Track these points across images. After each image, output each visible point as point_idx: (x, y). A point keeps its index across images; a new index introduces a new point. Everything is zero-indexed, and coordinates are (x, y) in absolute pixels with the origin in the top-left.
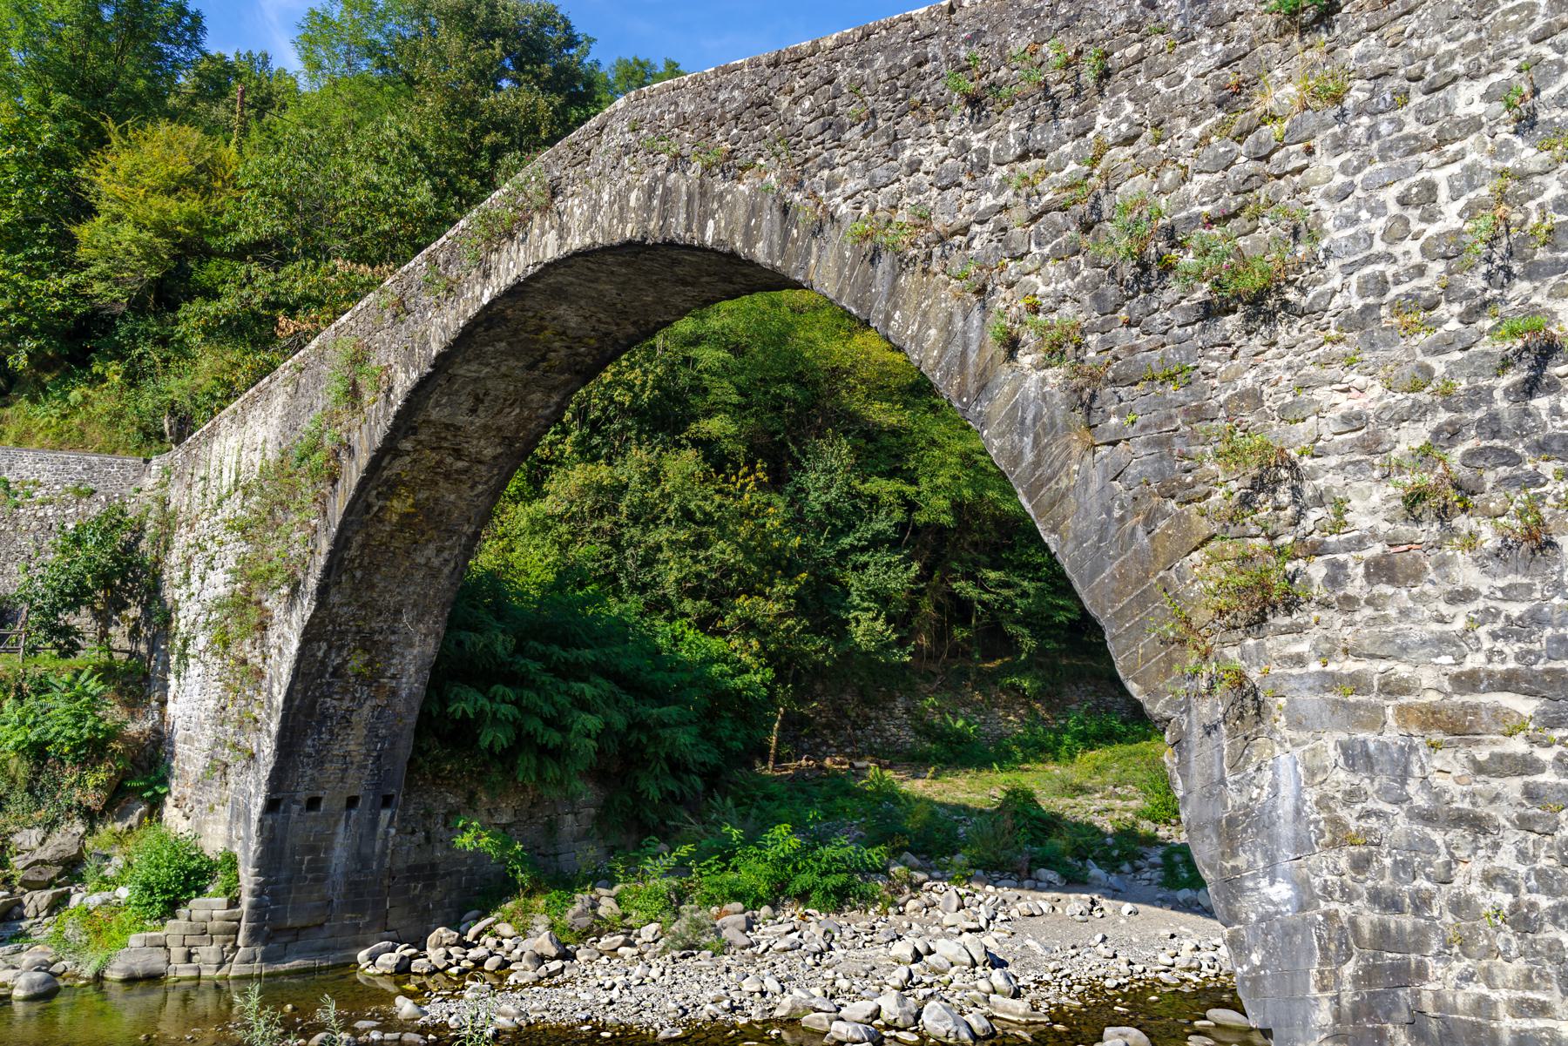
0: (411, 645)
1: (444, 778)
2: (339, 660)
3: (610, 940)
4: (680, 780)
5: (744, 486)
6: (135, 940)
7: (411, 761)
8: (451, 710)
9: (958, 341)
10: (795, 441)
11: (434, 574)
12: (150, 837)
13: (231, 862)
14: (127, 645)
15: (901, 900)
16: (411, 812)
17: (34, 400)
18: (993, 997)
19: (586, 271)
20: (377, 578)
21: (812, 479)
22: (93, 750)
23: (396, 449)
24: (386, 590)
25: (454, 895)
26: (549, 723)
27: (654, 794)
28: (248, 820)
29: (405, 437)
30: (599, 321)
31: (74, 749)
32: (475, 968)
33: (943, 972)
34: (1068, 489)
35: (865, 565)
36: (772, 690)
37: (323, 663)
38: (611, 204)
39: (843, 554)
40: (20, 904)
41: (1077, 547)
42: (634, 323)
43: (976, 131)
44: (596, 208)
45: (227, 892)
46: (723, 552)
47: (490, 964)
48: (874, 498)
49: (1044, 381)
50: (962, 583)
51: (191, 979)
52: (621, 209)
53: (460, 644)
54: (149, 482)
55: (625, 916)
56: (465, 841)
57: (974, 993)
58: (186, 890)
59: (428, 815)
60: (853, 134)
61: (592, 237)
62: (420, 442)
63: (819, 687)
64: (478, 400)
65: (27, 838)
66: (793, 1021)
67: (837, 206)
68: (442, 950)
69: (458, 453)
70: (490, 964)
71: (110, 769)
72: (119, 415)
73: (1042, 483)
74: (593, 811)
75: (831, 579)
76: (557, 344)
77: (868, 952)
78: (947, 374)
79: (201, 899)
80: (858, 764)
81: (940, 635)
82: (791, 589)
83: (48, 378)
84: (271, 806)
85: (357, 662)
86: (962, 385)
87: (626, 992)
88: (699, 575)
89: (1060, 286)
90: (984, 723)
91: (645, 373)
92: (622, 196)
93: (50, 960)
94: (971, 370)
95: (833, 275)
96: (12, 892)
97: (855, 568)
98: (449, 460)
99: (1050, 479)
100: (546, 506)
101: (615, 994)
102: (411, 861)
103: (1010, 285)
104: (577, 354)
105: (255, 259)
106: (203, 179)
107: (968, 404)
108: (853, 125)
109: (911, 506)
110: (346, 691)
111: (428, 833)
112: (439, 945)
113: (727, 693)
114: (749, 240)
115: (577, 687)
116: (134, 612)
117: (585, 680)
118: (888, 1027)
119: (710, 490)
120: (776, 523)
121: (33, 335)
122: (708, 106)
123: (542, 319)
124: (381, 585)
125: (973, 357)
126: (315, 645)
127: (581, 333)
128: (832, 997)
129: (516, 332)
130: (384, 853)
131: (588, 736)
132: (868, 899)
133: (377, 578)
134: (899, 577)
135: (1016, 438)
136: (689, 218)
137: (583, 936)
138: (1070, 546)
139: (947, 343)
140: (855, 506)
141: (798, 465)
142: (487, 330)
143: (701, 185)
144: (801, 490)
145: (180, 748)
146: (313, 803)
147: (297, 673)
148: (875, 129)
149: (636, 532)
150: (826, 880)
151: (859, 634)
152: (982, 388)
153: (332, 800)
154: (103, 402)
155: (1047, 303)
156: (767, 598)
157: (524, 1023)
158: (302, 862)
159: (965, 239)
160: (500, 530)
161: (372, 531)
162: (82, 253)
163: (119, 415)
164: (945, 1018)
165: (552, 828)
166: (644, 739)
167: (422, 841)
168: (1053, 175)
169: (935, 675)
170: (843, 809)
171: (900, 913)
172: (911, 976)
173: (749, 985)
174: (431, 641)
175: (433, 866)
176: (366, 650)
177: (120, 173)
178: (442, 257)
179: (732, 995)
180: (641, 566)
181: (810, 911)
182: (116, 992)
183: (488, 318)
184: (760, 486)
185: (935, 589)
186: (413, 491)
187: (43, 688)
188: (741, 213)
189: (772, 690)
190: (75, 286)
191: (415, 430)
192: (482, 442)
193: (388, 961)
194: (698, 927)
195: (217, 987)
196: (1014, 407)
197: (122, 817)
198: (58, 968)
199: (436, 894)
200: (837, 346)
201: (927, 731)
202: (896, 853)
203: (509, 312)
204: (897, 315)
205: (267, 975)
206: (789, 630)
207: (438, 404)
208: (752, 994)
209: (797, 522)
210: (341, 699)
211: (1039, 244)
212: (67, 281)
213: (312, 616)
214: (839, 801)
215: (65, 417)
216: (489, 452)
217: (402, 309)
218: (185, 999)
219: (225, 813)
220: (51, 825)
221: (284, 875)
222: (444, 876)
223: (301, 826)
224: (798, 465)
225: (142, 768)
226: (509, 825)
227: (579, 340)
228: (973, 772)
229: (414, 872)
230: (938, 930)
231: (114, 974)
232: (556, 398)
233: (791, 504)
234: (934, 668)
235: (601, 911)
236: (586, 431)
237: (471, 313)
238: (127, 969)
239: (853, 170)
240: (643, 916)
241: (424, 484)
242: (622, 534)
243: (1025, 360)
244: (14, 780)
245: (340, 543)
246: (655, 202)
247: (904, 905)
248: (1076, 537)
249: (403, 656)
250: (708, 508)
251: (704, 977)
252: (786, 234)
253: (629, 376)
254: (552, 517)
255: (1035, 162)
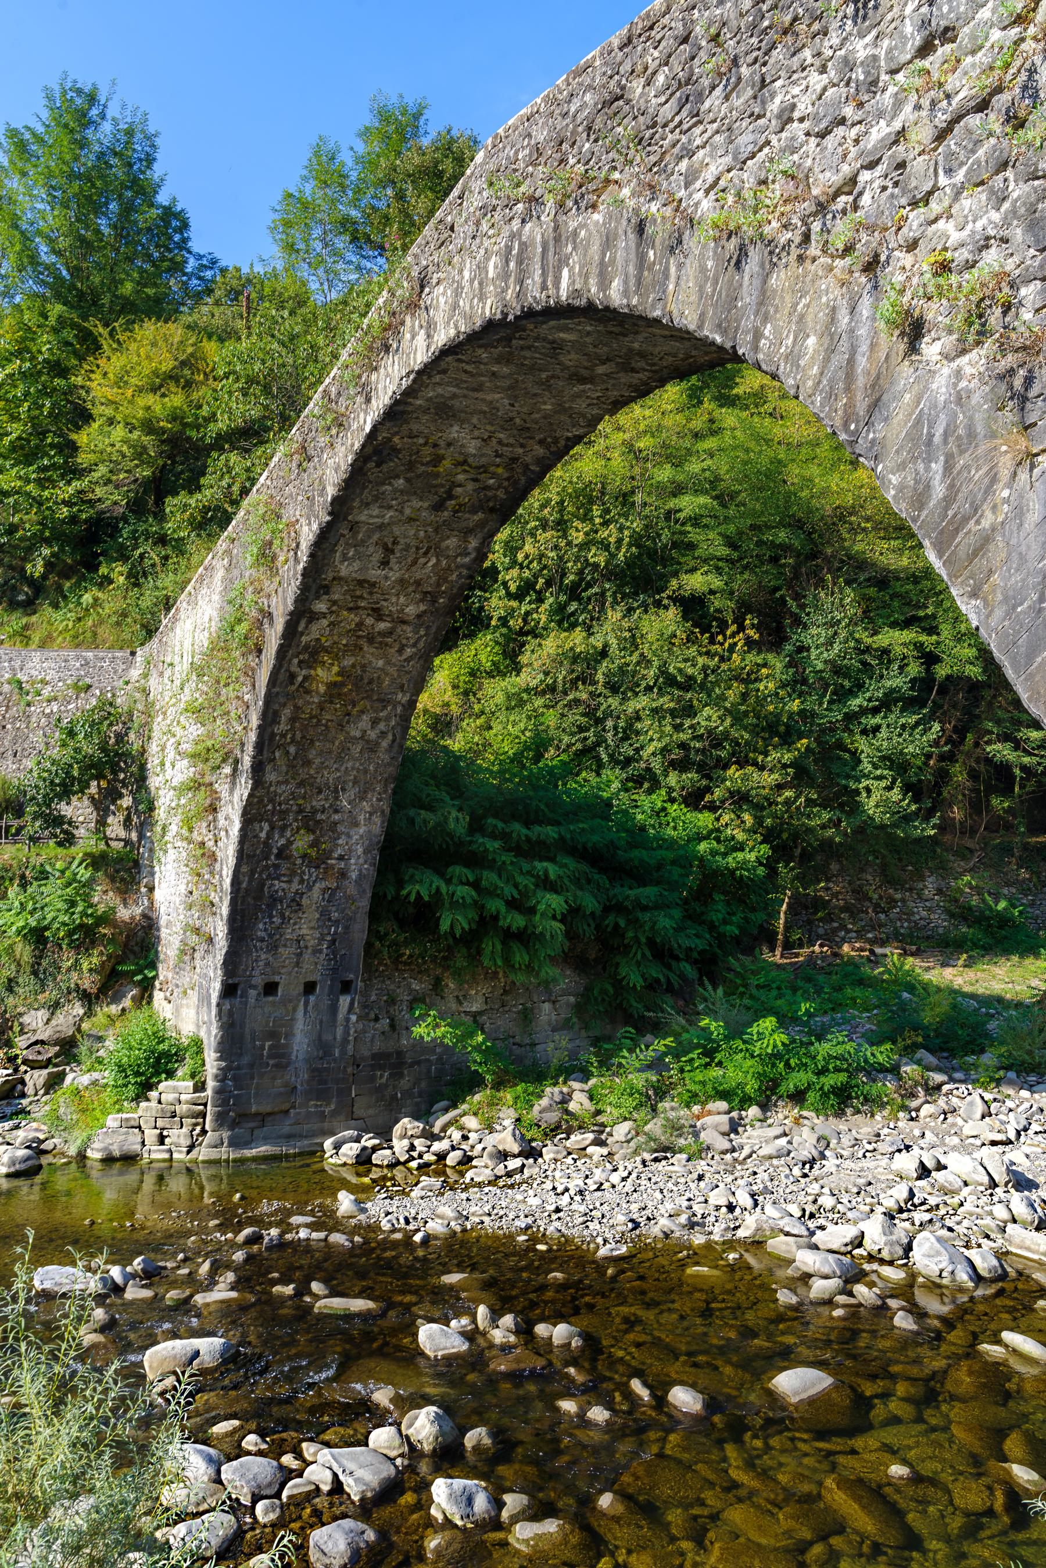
0: (356, 824)
1: (405, 963)
2: (282, 841)
3: (580, 1137)
4: (669, 967)
5: (732, 648)
6: (112, 1121)
7: (369, 946)
8: (404, 892)
9: (844, 346)
10: (797, 597)
11: (372, 747)
12: (137, 1024)
13: (198, 1045)
14: (122, 834)
15: (914, 1104)
16: (373, 998)
17: (56, 606)
18: (1010, 1228)
19: (464, 377)
20: (312, 754)
21: (815, 634)
22: (85, 936)
23: (311, 612)
24: (322, 766)
25: (423, 1085)
26: (513, 904)
27: (635, 979)
28: (209, 1004)
29: (318, 598)
30: (500, 442)
31: (70, 933)
32: (437, 1162)
33: (953, 1192)
34: (993, 529)
35: (877, 729)
36: (772, 872)
37: (266, 843)
38: (472, 281)
39: (851, 717)
40: (23, 1083)
41: (1008, 615)
42: (541, 442)
43: (862, 35)
44: (457, 293)
45: (193, 1076)
46: (709, 719)
47: (452, 1159)
48: (886, 651)
49: (958, 374)
50: (998, 746)
51: (164, 1160)
52: (481, 284)
53: (412, 821)
54: (135, 673)
55: (598, 1112)
56: (420, 1030)
57: (988, 1221)
58: (157, 1073)
59: (392, 1001)
60: (713, 101)
61: (456, 327)
62: (334, 603)
63: (834, 867)
64: (388, 551)
65: (36, 1020)
66: (759, 1243)
67: (697, 204)
68: (406, 1142)
69: (378, 614)
70: (452, 1159)
71: (101, 954)
72: (124, 615)
73: (958, 525)
74: (572, 999)
75: (840, 746)
76: (461, 477)
77: (864, 1163)
78: (831, 396)
79: (170, 1083)
80: (879, 951)
81: (977, 805)
82: (787, 757)
83: (68, 584)
84: (229, 991)
85: (301, 843)
86: (850, 406)
87: (578, 1198)
88: (683, 746)
89: (979, 225)
90: (1032, 904)
91: (621, 529)
92: (482, 268)
93: (42, 1137)
94: (861, 381)
95: (694, 298)
96: (16, 1070)
97: (864, 732)
98: (370, 621)
99: (966, 519)
100: (527, 678)
101: (566, 1198)
102: (376, 1049)
103: (912, 246)
104: (487, 488)
105: (233, 448)
106: (184, 374)
107: (857, 433)
108: (713, 88)
109: (930, 659)
110: (293, 873)
111: (392, 1020)
112: (403, 1136)
113: (717, 873)
114: (604, 284)
115: (540, 866)
116: (127, 801)
117: (552, 860)
118: (871, 1258)
119: (692, 651)
120: (771, 685)
121: (48, 542)
122: (560, 123)
123: (435, 445)
124: (318, 761)
125: (862, 362)
126: (257, 826)
127: (484, 461)
128: (812, 1216)
129: (411, 466)
130: (345, 1041)
131: (554, 917)
132: (873, 1103)
133: (312, 754)
134: (919, 739)
135: (921, 467)
136: (544, 275)
137: (552, 1132)
138: (999, 613)
139: (831, 351)
140: (864, 663)
141: (797, 621)
142: (378, 465)
143: (556, 228)
144: (801, 649)
145: (164, 933)
146: (271, 988)
147: (242, 855)
148: (739, 79)
149: (614, 702)
150: (823, 1079)
151: (870, 805)
152: (875, 405)
153: (289, 985)
154: (111, 602)
155: (963, 255)
156: (762, 768)
157: (458, 1229)
158: (262, 1048)
159: (851, 198)
160: (477, 707)
161: (300, 703)
162: (83, 459)
163: (124, 615)
164: (938, 1254)
165: (527, 1016)
166: (622, 923)
167: (387, 1028)
168: (969, 59)
169: (971, 851)
170: (854, 999)
171: (912, 1119)
172: (912, 1194)
173: (717, 1198)
174: (377, 819)
175: (400, 1054)
176: (310, 831)
177: (111, 376)
178: (333, 390)
179: (696, 1208)
180: (623, 739)
181: (805, 1113)
182: (95, 1168)
183: (374, 453)
184: (749, 642)
185: (969, 755)
186: (336, 658)
187: (43, 875)
188: (595, 248)
189: (772, 871)
190: (80, 492)
191: (326, 589)
192: (402, 599)
193: (350, 1150)
194: (676, 1128)
195: (188, 1170)
196: (918, 422)
197: (116, 999)
198: (47, 1146)
199: (405, 1083)
200: (834, 482)
201: (963, 914)
202: (909, 1051)
203: (396, 439)
204: (768, 330)
205: (235, 1161)
206: (788, 802)
207: (345, 558)
208: (718, 1208)
209: (798, 684)
210: (289, 882)
211: (949, 172)
212: (76, 484)
213: (250, 795)
214: (849, 991)
215: (79, 619)
216: (411, 610)
217: (305, 455)
218: (161, 1178)
219: (193, 996)
220: (54, 1007)
221: (246, 1060)
222: (412, 1065)
223: (260, 1013)
224: (797, 621)
225: (134, 953)
226: (481, 1013)
227: (483, 469)
228: (1015, 958)
229: (380, 1060)
230: (956, 1140)
231: (94, 1154)
232: (473, 543)
233: (789, 665)
234: (970, 843)
235: (572, 1106)
236: (563, 598)
237: (357, 446)
238: (105, 1149)
239: (714, 148)
240: (616, 1113)
241: (347, 650)
242: (600, 704)
243: (931, 349)
244: (19, 965)
245: (269, 717)
246: (512, 265)
247: (917, 1110)
248: (1006, 599)
249: (349, 836)
250: (690, 671)
251: (670, 1185)
252: (642, 257)
253: (603, 534)
254: (527, 690)
255: (943, 51)
